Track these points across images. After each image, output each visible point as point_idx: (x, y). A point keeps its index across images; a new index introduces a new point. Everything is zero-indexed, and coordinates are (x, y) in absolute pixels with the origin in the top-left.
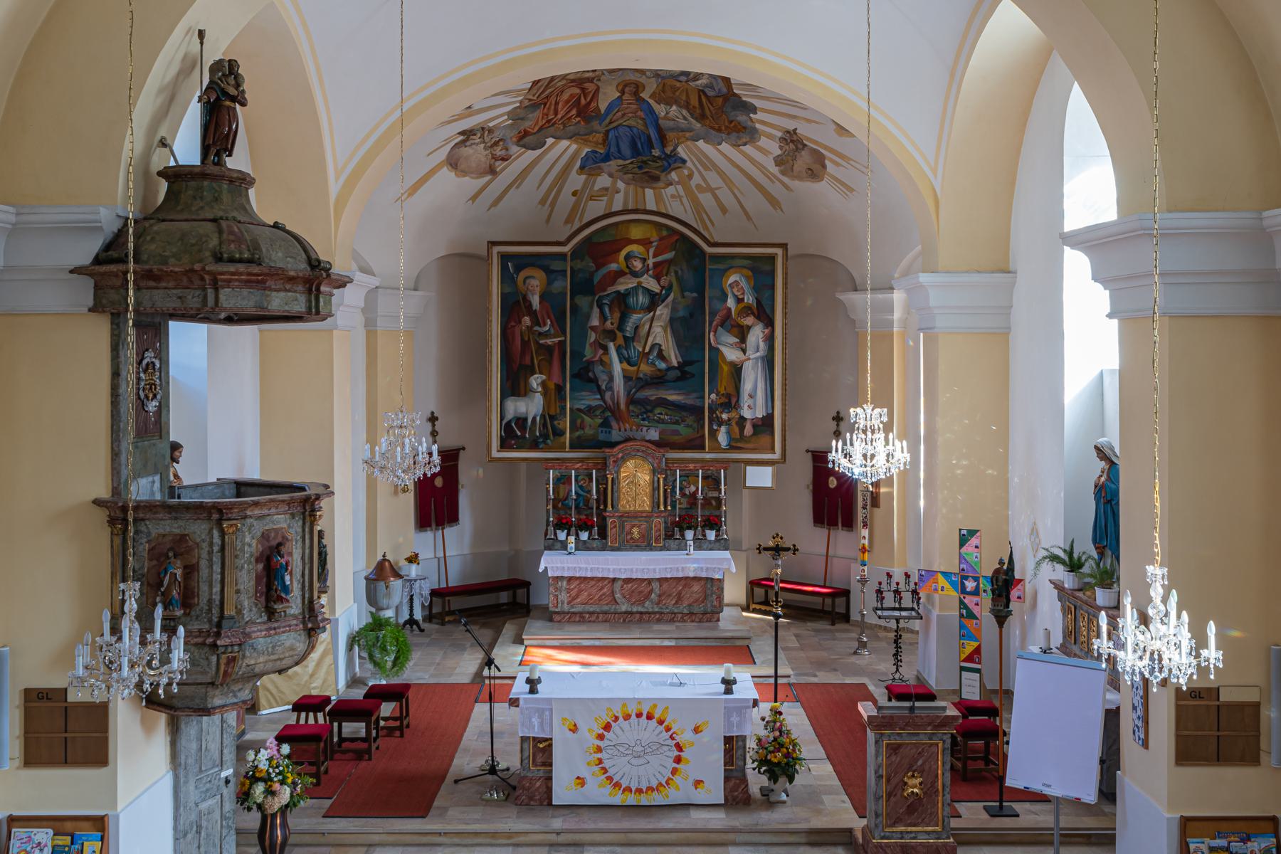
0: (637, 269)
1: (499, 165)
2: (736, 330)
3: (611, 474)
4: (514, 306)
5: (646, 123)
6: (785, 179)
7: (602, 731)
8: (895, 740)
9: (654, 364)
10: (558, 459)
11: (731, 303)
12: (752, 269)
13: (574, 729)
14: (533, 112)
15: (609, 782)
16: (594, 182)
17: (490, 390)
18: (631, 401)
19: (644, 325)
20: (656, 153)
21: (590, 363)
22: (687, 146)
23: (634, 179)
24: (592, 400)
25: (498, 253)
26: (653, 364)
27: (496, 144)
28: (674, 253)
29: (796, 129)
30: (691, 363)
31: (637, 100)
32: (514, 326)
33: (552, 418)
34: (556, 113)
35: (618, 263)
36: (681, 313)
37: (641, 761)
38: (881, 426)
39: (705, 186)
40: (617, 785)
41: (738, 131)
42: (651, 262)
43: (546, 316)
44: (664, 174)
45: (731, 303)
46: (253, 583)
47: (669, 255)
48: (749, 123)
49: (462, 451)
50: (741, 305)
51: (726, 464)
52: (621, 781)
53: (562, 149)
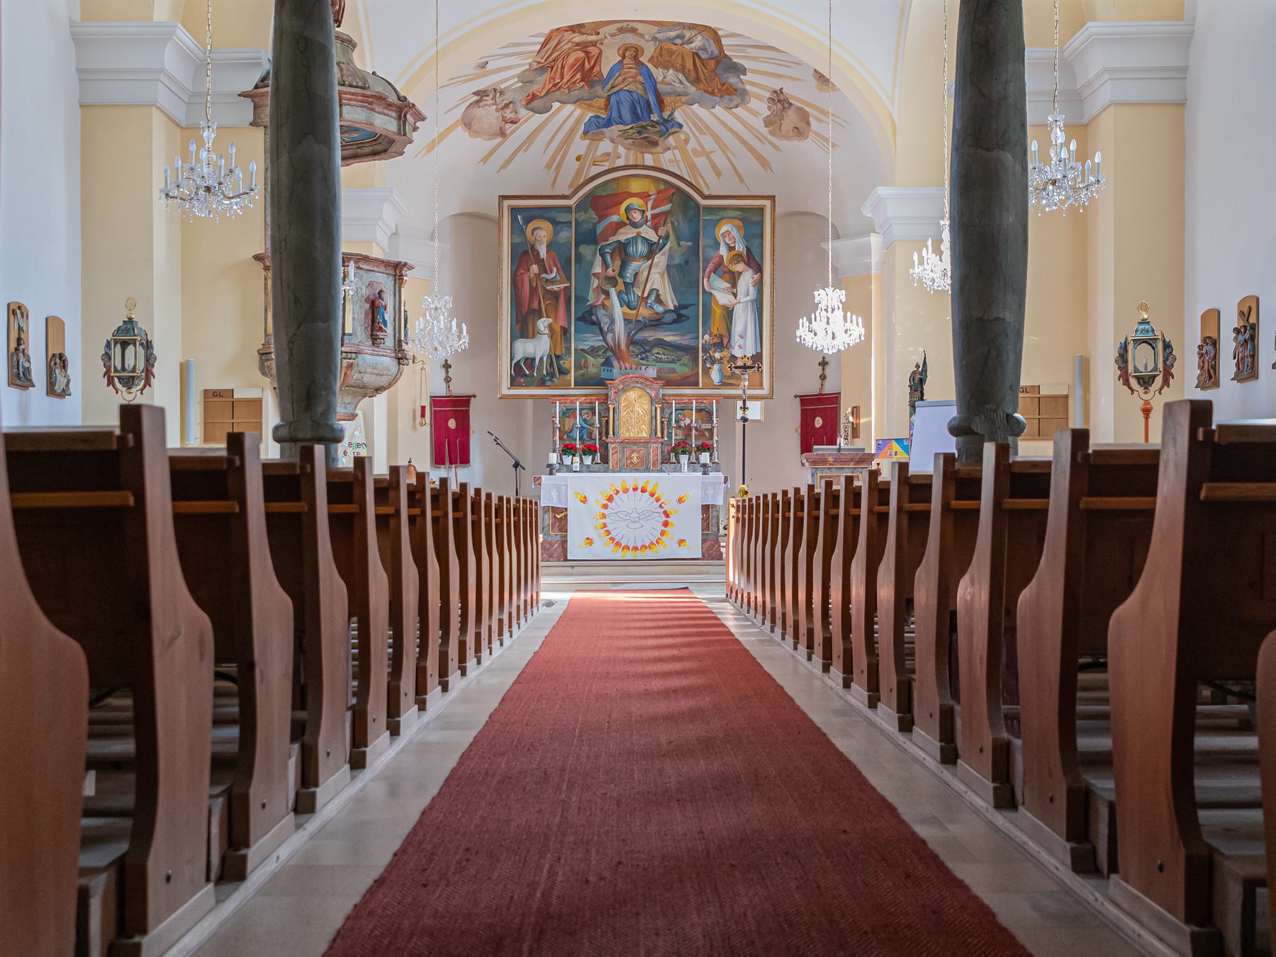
0: (637, 221)
1: (509, 128)
2: (727, 276)
3: (613, 404)
4: (523, 255)
5: (645, 88)
6: (771, 138)
7: (606, 502)
8: (826, 473)
9: (652, 308)
10: (563, 396)
11: (723, 251)
12: (742, 220)
13: (584, 500)
14: (540, 75)
15: (611, 542)
16: (597, 147)
17: (500, 332)
18: (631, 342)
19: (643, 272)
20: (655, 117)
21: (593, 307)
22: (684, 111)
23: (633, 144)
24: (593, 341)
25: (509, 206)
26: (651, 307)
27: (506, 106)
28: (671, 204)
29: (782, 88)
30: (686, 307)
31: (637, 64)
32: (524, 274)
33: (558, 357)
34: (562, 78)
35: (619, 215)
36: (677, 261)
37: (637, 525)
38: (841, 306)
39: (700, 150)
40: (618, 544)
41: (730, 94)
42: (649, 214)
43: (552, 264)
44: (662, 139)
45: (723, 251)
46: (363, 315)
47: (667, 207)
48: (740, 85)
49: (472, 398)
50: (733, 253)
51: (720, 398)
52: (621, 541)
53: (568, 114)
